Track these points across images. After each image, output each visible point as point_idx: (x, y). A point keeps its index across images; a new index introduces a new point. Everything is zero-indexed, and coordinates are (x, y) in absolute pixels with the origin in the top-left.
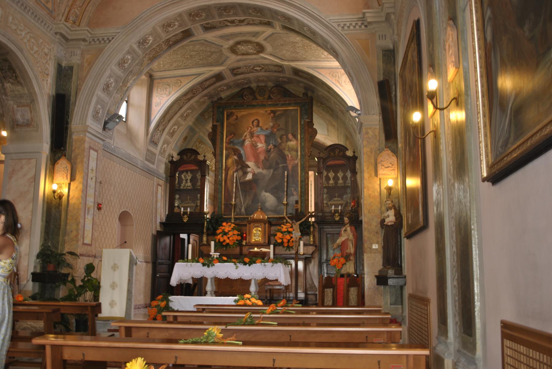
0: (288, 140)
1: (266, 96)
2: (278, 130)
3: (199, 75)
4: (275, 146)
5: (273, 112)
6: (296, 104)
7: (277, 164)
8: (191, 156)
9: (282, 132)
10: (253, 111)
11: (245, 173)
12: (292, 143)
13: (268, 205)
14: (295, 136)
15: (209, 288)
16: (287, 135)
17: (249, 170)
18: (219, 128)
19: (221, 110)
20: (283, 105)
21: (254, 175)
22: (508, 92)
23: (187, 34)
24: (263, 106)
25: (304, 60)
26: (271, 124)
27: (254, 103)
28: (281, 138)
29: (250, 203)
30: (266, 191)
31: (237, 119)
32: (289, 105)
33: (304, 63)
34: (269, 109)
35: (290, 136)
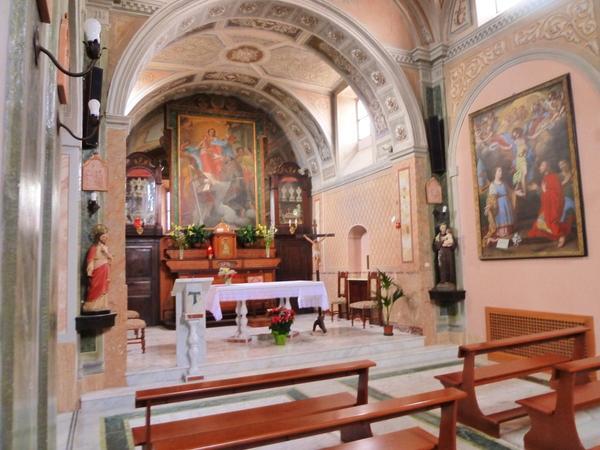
0: (244, 154)
1: (222, 106)
2: (235, 143)
3: (188, 70)
4: (232, 159)
5: (229, 123)
6: (252, 119)
7: (235, 176)
8: (143, 161)
9: (239, 145)
10: (206, 119)
11: (203, 184)
12: (247, 158)
13: (226, 217)
14: (250, 150)
15: (244, 311)
16: (243, 149)
17: (206, 180)
18: (173, 134)
19: (174, 113)
20: (239, 118)
21: (211, 186)
22: (196, 120)
23: (210, 26)
24: (219, 116)
25: (290, 78)
26: (228, 136)
27: (210, 111)
28: (238, 150)
29: (208, 215)
30: (225, 204)
31: (191, 125)
32: (245, 118)
33: (283, 80)
34: (225, 120)
35: (246, 149)
